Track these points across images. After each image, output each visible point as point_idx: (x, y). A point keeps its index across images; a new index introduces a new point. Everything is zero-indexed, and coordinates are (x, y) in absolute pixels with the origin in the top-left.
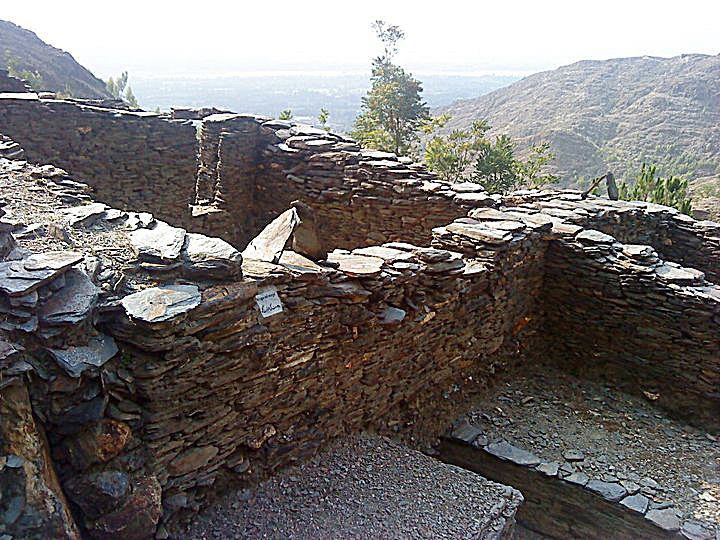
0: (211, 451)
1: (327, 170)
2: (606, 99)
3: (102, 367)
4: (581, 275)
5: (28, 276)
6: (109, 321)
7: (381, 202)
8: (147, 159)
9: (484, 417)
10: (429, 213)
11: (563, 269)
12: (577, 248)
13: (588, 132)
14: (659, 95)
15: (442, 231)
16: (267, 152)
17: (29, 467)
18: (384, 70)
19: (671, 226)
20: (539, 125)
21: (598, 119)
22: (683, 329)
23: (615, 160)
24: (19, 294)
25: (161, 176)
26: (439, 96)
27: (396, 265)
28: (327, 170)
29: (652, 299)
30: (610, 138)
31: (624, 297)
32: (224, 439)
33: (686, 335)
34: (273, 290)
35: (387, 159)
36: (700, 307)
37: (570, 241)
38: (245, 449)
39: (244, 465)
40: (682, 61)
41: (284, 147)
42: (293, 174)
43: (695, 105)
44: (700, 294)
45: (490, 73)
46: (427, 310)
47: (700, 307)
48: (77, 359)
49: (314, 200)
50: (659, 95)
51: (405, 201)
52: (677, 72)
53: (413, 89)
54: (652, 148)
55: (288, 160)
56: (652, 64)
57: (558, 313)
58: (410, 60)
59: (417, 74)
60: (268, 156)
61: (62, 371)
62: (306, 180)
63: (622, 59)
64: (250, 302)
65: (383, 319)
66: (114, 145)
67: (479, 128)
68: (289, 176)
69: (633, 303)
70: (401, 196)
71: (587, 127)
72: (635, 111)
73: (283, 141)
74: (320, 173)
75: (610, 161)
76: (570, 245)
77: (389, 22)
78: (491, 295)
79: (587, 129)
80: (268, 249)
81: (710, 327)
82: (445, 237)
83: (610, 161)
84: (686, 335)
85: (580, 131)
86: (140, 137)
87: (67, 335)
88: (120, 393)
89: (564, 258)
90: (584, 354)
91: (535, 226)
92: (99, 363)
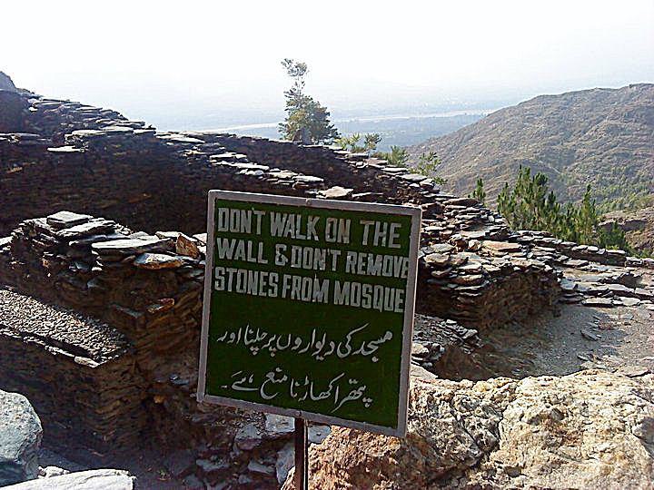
2: (564, 129)
14: (613, 122)
18: (297, 101)
20: (505, 155)
21: (558, 147)
23: (575, 183)
26: (417, 136)
30: (569, 163)
40: (630, 90)
41: (32, 109)
43: (644, 130)
45: (462, 113)
50: (613, 122)
52: (626, 101)
53: (322, 114)
54: (609, 170)
56: (602, 96)
58: (317, 89)
59: (323, 100)
63: (576, 92)
67: (371, 140)
71: (548, 154)
72: (590, 138)
75: (570, 185)
77: (298, 59)
79: (548, 156)
83: (570, 185)
85: (541, 159)
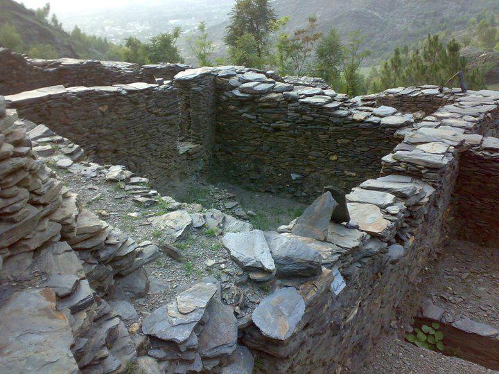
1: (274, 108)
5: (186, 321)
7: (320, 130)
8: (149, 121)
9: (442, 297)
10: (360, 135)
11: (474, 172)
12: (485, 155)
13: (376, 8)
16: (224, 98)
25: (159, 132)
28: (274, 108)
37: (478, 150)
41: (237, 93)
42: (247, 113)
46: (409, 236)
49: (265, 131)
55: (241, 103)
57: (470, 203)
60: (225, 101)
66: (125, 116)
68: (244, 115)
70: (336, 125)
74: (269, 110)
76: (479, 153)
86: (141, 106)
89: (474, 163)
90: (492, 230)
91: (456, 144)
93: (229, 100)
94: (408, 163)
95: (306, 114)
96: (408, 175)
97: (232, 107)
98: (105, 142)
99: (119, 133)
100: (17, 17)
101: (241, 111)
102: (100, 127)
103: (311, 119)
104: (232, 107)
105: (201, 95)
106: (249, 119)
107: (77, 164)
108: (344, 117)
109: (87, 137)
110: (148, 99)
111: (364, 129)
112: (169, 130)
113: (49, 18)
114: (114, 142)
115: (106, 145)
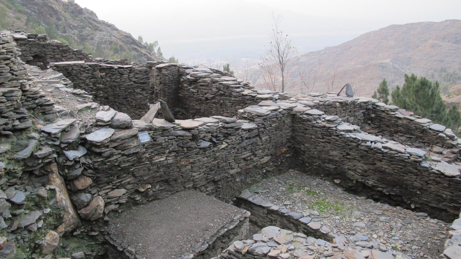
0: (123, 191)
3: (81, 157)
4: (307, 129)
6: (83, 142)
12: (304, 117)
15: (241, 111)
17: (57, 189)
19: (374, 108)
22: (347, 151)
24: (55, 134)
27: (208, 124)
29: (334, 139)
31: (323, 138)
32: (129, 187)
33: (348, 154)
34: (146, 133)
35: (227, 81)
36: (352, 142)
38: (137, 192)
39: (138, 198)
41: (188, 77)
42: (193, 88)
44: (228, 119)
47: (352, 142)
48: (71, 154)
51: (236, 99)
61: (68, 159)
62: (198, 91)
64: (135, 136)
65: (199, 146)
69: (327, 140)
73: (188, 74)
78: (260, 138)
80: (152, 118)
81: (357, 150)
82: (242, 113)
84: (348, 154)
87: (72, 146)
88: (87, 166)
91: (285, 108)
92: (80, 156)
93: (184, 81)
94: (249, 113)
95: (221, 90)
96: (249, 119)
97: (185, 85)
98: (101, 92)
99: (110, 89)
100: (135, 49)
101: (189, 88)
102: (99, 84)
103: (223, 93)
104: (185, 85)
105: (167, 76)
106: (193, 92)
107: (265, 252)
108: (238, 92)
109: (91, 88)
110: (130, 73)
111: (248, 100)
112: (141, 92)
113: (156, 50)
114: (106, 93)
115: (101, 94)
